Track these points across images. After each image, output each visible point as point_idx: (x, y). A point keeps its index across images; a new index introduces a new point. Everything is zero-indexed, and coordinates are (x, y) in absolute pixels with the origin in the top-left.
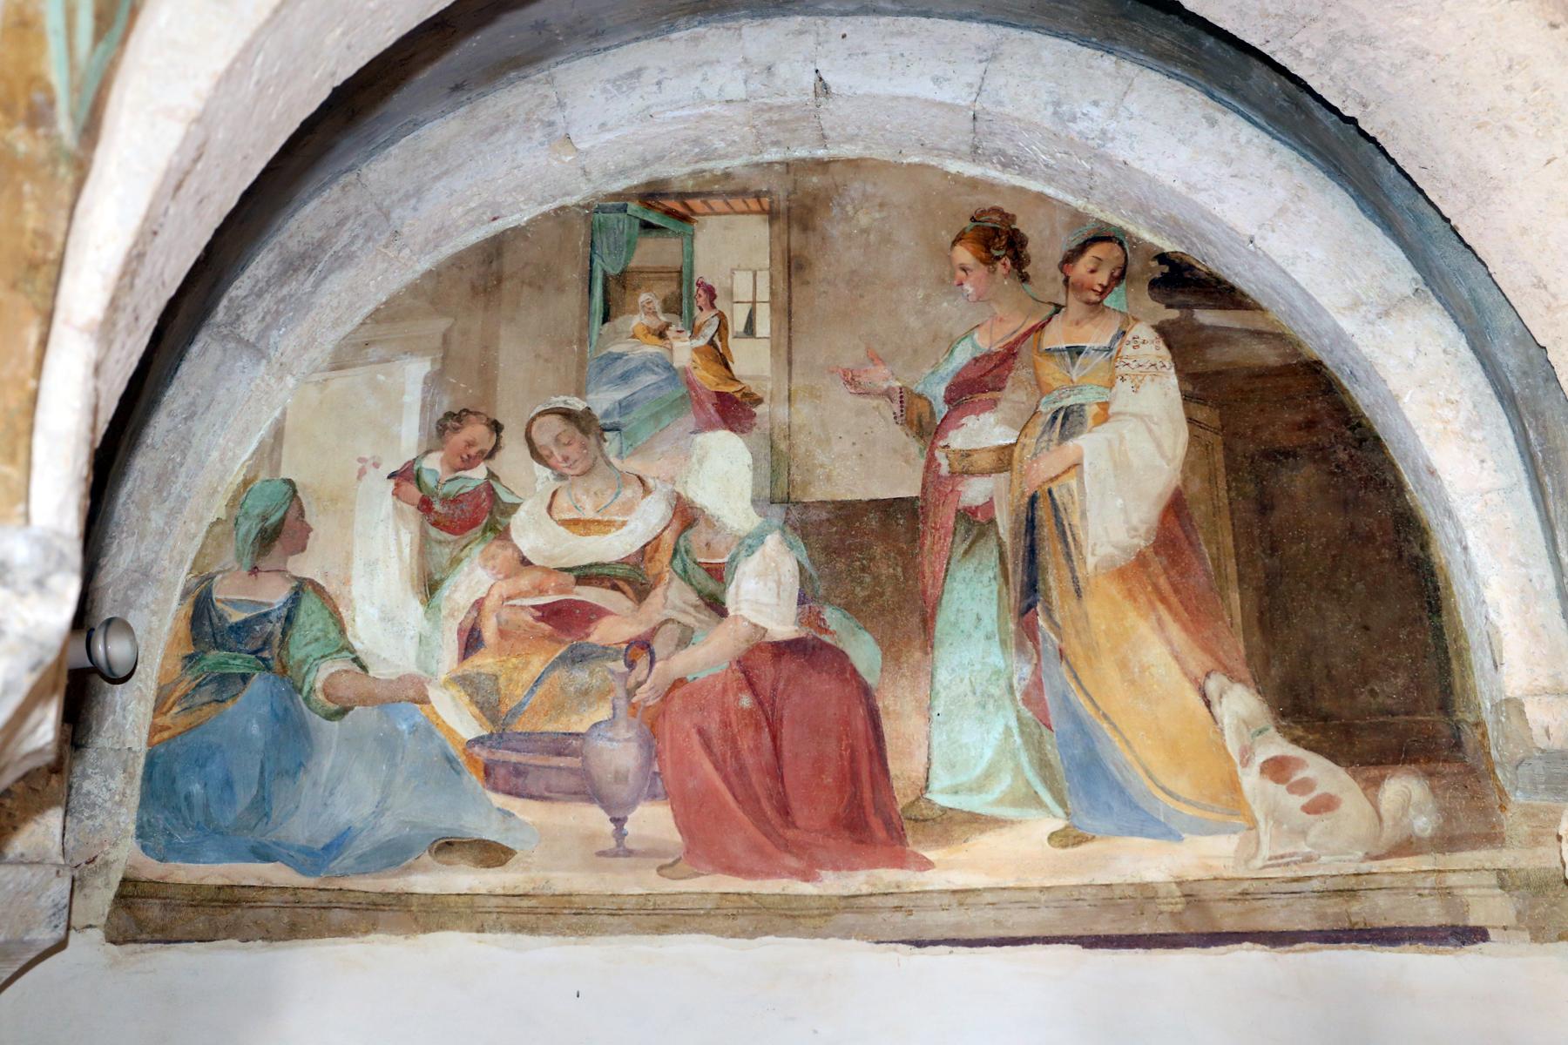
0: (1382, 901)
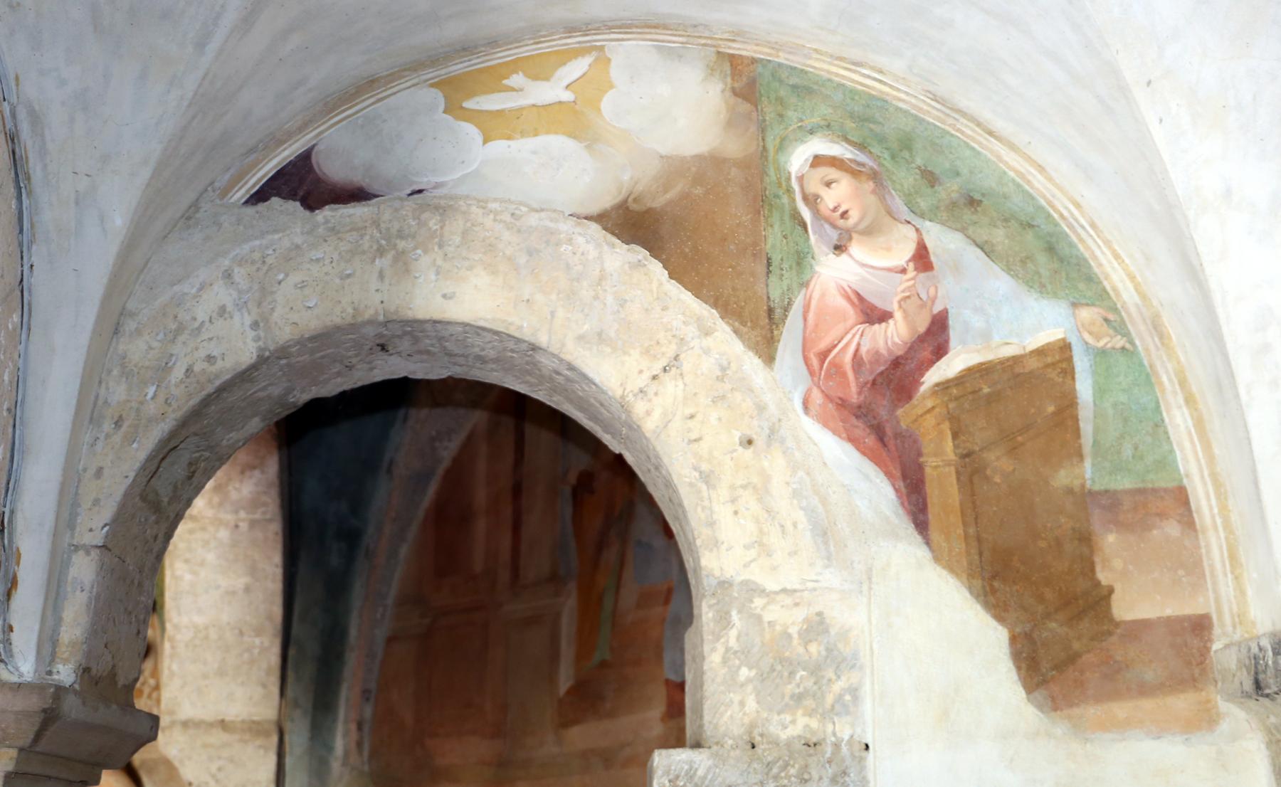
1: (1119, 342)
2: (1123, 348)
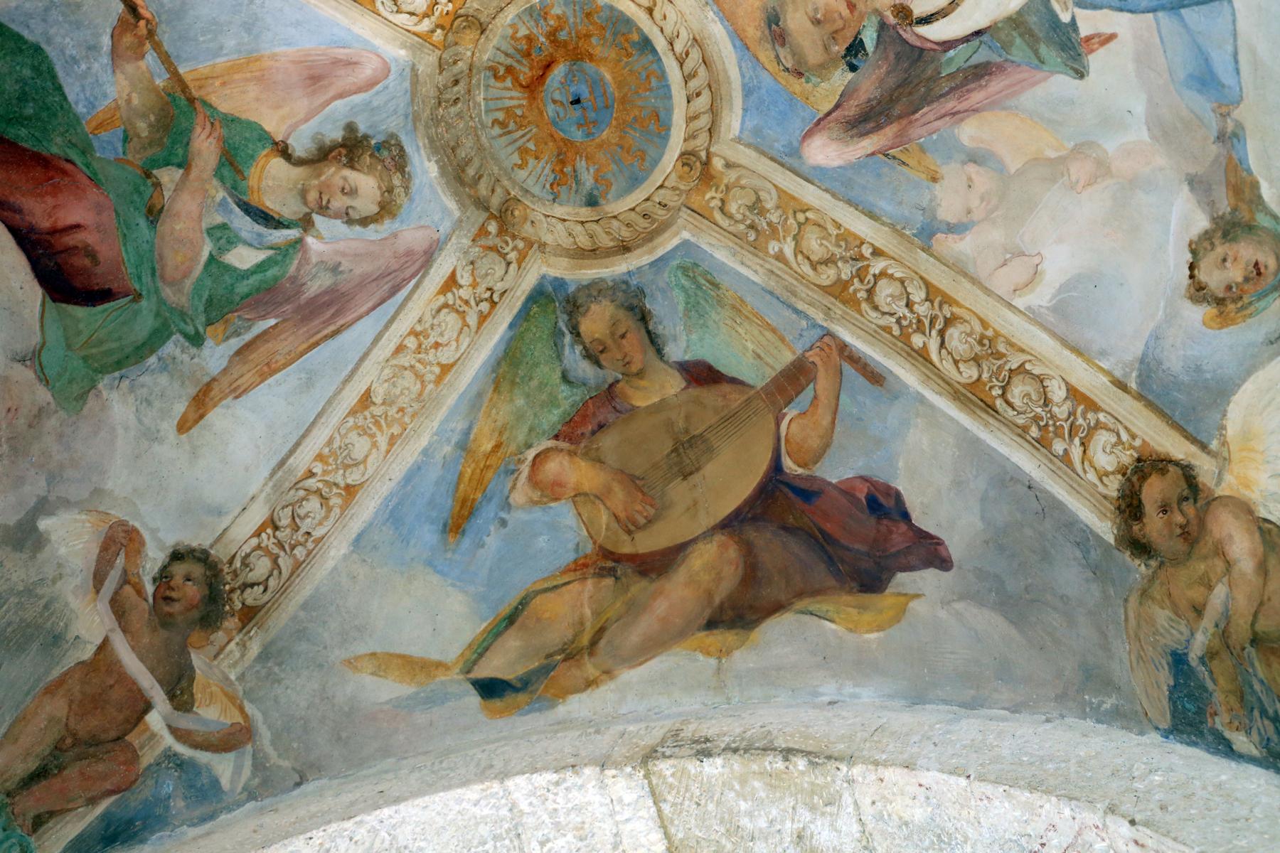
0: (23, 132)
1: (819, 332)
2: (1083, 444)
